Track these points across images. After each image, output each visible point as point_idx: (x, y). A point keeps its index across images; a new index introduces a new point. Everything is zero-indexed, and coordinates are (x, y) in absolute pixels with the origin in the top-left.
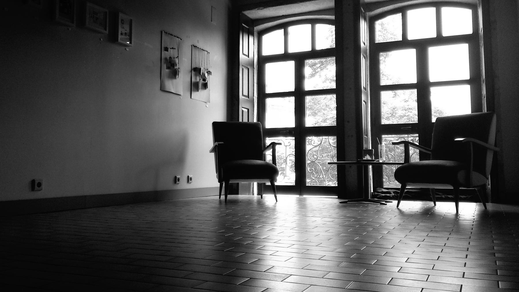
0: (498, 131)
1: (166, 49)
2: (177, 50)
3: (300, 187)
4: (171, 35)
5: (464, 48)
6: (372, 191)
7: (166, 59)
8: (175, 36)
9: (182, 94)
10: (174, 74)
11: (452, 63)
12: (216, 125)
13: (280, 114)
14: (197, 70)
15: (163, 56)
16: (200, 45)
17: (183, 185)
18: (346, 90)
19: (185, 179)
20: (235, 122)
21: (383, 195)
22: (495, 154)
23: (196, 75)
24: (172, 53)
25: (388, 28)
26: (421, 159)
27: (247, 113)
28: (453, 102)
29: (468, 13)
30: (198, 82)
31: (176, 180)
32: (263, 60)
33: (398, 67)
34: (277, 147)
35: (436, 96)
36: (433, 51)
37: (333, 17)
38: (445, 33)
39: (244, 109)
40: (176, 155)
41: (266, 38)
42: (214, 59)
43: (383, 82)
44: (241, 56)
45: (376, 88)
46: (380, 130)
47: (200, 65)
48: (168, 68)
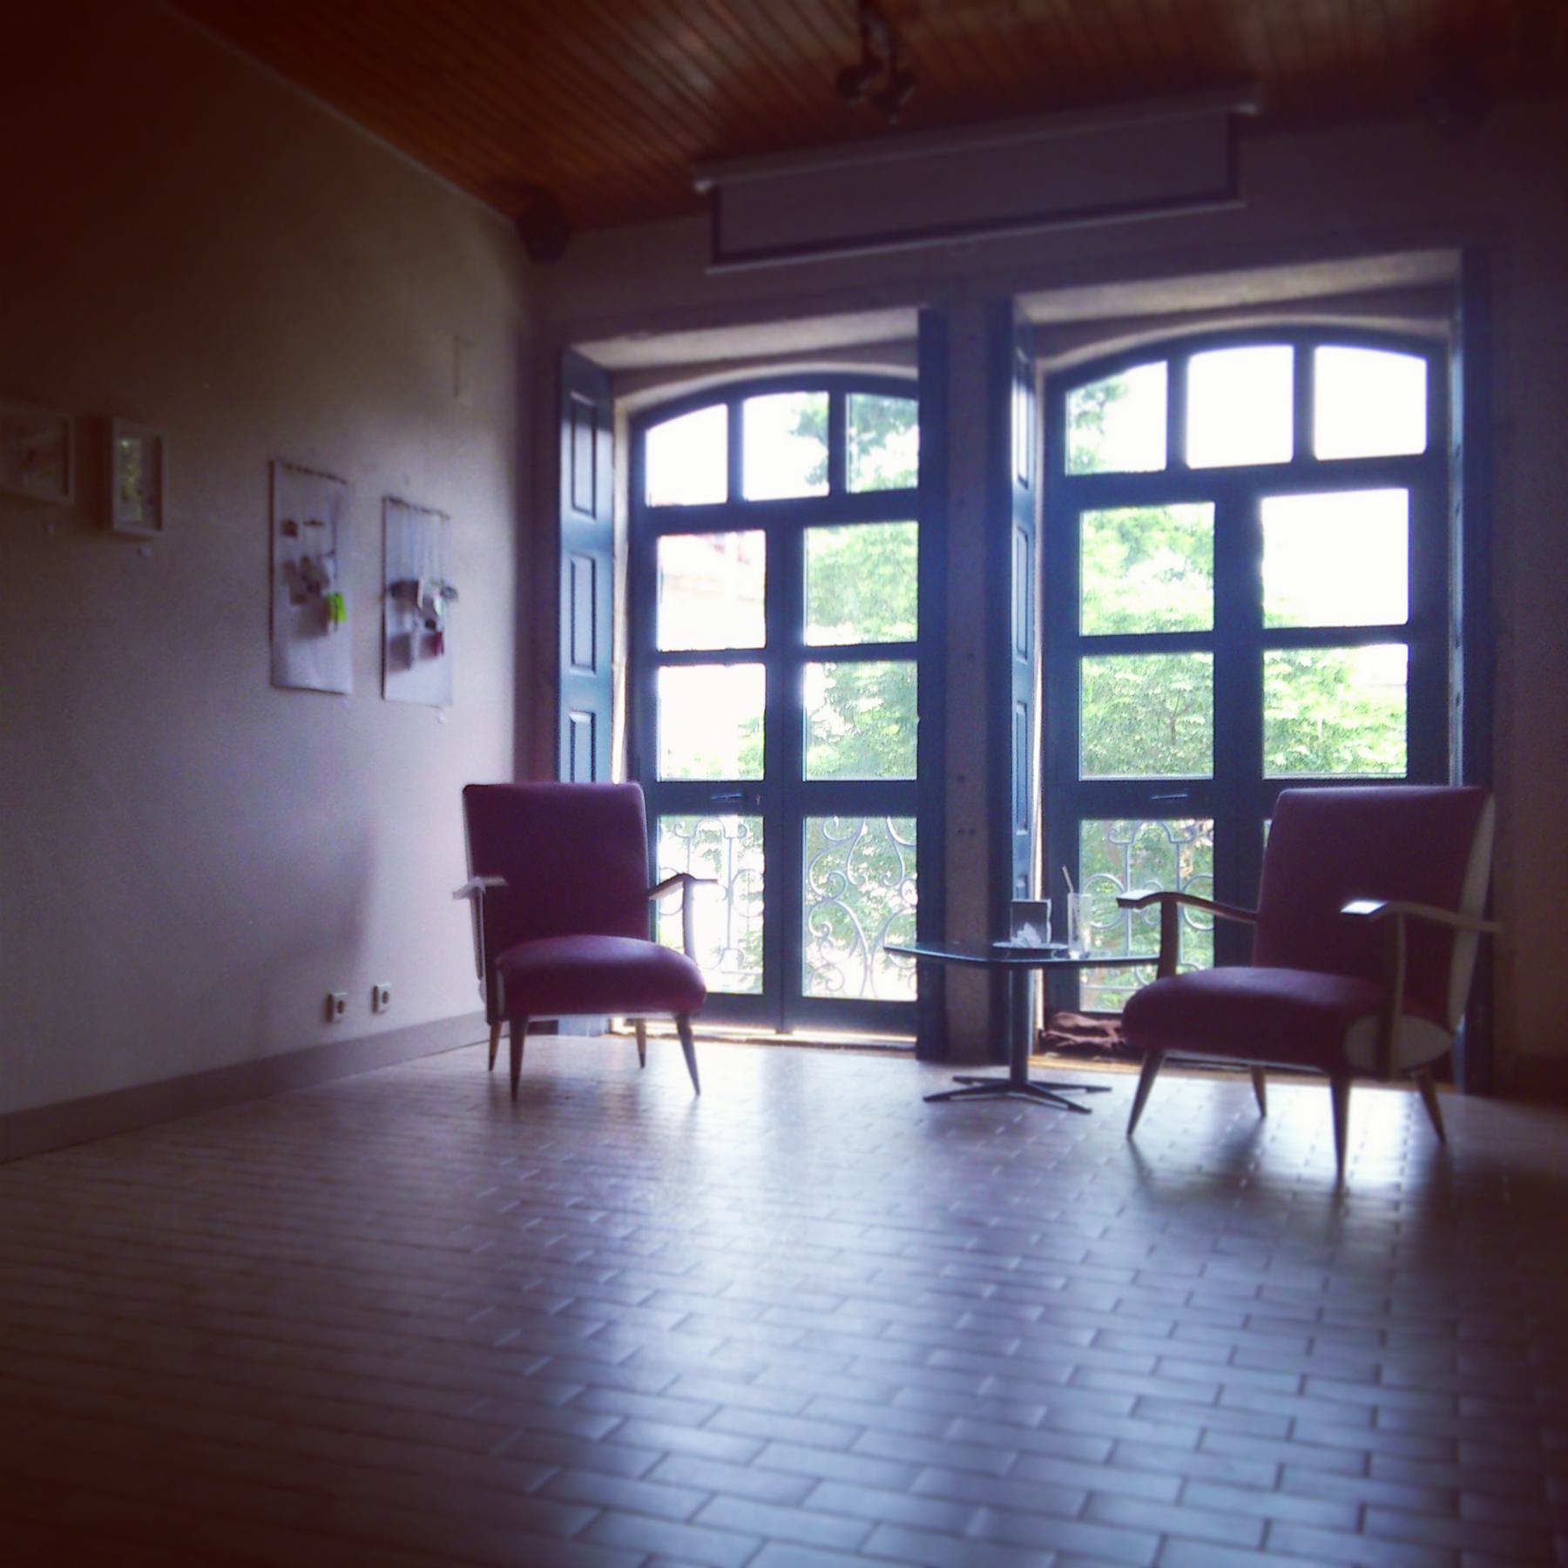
0: (1501, 832)
1: (291, 530)
2: (328, 527)
3: (780, 996)
4: (308, 471)
5: (1393, 504)
6: (1040, 1025)
7: (289, 566)
8: (321, 475)
9: (347, 685)
10: (319, 614)
11: (1345, 560)
12: (476, 796)
13: (709, 727)
14: (403, 591)
15: (279, 557)
16: (414, 492)
17: (357, 1023)
18: (955, 658)
19: (366, 1000)
20: (544, 783)
21: (1080, 1039)
22: (1487, 948)
23: (400, 610)
24: (310, 540)
25: (1117, 424)
26: (1221, 958)
27: (595, 759)
28: (1347, 720)
29: (1411, 371)
30: (410, 638)
31: (331, 1008)
32: (652, 524)
33: (1145, 572)
34: (697, 890)
35: (1286, 687)
36: (1278, 515)
37: (911, 372)
38: (1326, 449)
39: (577, 717)
40: (332, 925)
41: (658, 438)
42: (464, 541)
43: (1092, 623)
44: (567, 515)
45: (1067, 645)
46: (1078, 799)
47: (416, 570)
48: (298, 599)
